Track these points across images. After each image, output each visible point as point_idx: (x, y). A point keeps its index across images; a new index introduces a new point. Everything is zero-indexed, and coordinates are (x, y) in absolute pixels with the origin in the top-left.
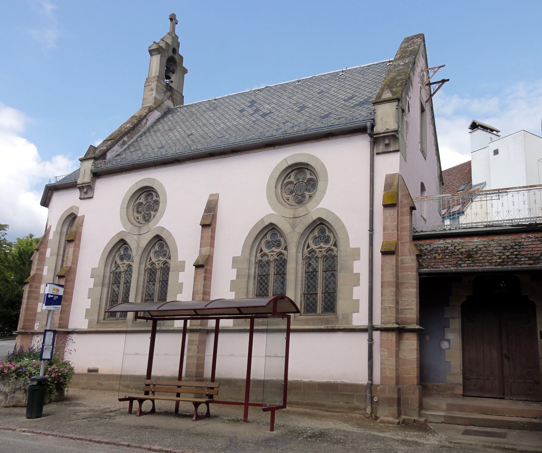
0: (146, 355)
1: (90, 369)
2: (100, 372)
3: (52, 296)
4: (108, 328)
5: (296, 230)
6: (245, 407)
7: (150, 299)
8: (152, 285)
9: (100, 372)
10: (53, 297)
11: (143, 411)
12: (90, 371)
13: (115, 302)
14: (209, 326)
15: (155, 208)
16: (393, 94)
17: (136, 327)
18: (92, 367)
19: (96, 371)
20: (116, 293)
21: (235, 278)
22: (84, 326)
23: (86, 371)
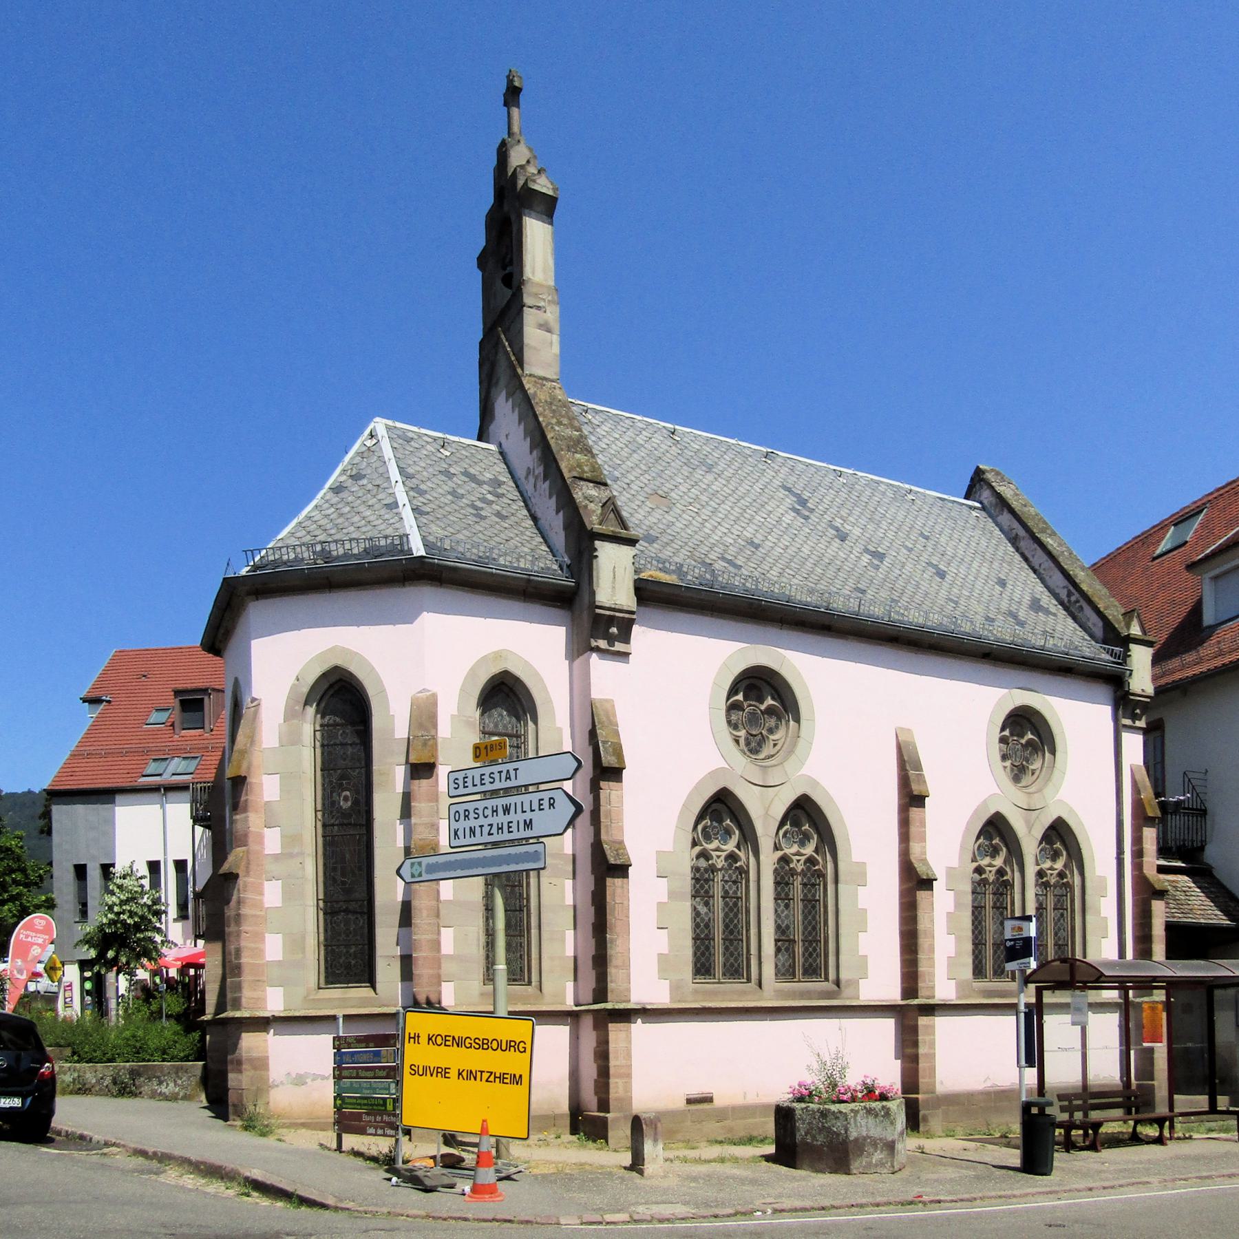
0: (327, 1078)
1: (692, 1096)
2: (718, 1102)
3: (1012, 943)
4: (711, 1001)
5: (1033, 832)
6: (1216, 1107)
7: (784, 938)
8: (782, 907)
9: (718, 1102)
10: (1015, 944)
11: (1156, 1126)
12: (690, 1101)
13: (703, 939)
14: (862, 998)
15: (767, 725)
16: (1144, 632)
17: (786, 1000)
18: (695, 1091)
19: (708, 1100)
20: (702, 920)
21: (952, 909)
22: (660, 996)
23: (677, 1102)
